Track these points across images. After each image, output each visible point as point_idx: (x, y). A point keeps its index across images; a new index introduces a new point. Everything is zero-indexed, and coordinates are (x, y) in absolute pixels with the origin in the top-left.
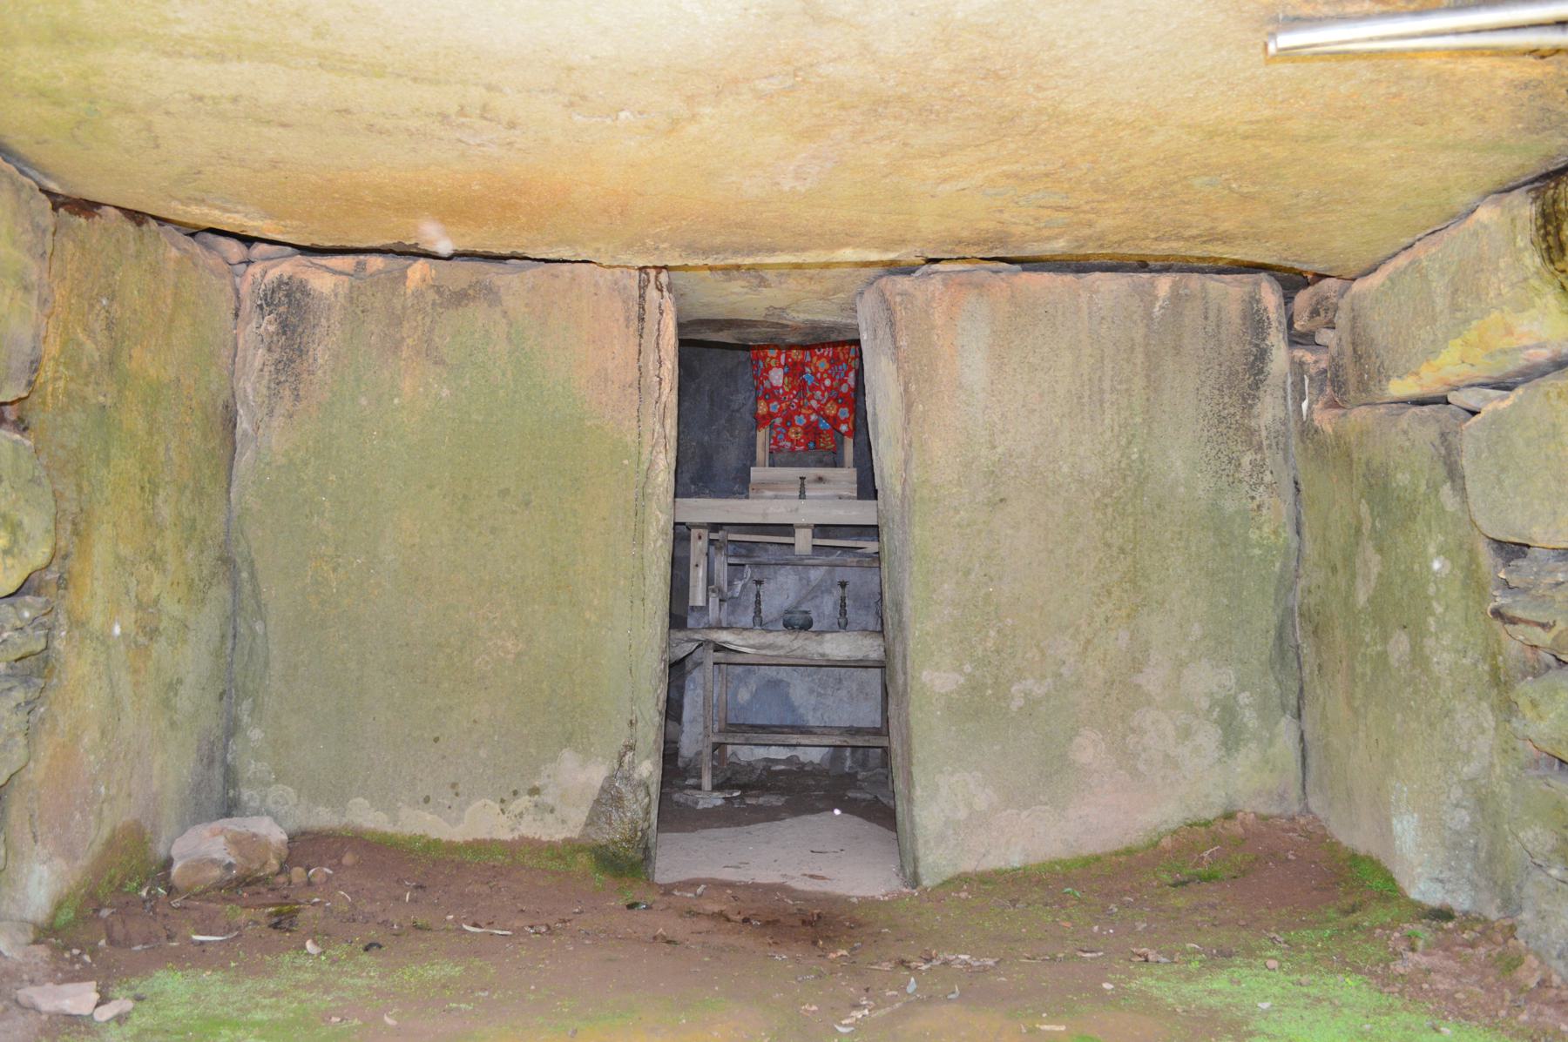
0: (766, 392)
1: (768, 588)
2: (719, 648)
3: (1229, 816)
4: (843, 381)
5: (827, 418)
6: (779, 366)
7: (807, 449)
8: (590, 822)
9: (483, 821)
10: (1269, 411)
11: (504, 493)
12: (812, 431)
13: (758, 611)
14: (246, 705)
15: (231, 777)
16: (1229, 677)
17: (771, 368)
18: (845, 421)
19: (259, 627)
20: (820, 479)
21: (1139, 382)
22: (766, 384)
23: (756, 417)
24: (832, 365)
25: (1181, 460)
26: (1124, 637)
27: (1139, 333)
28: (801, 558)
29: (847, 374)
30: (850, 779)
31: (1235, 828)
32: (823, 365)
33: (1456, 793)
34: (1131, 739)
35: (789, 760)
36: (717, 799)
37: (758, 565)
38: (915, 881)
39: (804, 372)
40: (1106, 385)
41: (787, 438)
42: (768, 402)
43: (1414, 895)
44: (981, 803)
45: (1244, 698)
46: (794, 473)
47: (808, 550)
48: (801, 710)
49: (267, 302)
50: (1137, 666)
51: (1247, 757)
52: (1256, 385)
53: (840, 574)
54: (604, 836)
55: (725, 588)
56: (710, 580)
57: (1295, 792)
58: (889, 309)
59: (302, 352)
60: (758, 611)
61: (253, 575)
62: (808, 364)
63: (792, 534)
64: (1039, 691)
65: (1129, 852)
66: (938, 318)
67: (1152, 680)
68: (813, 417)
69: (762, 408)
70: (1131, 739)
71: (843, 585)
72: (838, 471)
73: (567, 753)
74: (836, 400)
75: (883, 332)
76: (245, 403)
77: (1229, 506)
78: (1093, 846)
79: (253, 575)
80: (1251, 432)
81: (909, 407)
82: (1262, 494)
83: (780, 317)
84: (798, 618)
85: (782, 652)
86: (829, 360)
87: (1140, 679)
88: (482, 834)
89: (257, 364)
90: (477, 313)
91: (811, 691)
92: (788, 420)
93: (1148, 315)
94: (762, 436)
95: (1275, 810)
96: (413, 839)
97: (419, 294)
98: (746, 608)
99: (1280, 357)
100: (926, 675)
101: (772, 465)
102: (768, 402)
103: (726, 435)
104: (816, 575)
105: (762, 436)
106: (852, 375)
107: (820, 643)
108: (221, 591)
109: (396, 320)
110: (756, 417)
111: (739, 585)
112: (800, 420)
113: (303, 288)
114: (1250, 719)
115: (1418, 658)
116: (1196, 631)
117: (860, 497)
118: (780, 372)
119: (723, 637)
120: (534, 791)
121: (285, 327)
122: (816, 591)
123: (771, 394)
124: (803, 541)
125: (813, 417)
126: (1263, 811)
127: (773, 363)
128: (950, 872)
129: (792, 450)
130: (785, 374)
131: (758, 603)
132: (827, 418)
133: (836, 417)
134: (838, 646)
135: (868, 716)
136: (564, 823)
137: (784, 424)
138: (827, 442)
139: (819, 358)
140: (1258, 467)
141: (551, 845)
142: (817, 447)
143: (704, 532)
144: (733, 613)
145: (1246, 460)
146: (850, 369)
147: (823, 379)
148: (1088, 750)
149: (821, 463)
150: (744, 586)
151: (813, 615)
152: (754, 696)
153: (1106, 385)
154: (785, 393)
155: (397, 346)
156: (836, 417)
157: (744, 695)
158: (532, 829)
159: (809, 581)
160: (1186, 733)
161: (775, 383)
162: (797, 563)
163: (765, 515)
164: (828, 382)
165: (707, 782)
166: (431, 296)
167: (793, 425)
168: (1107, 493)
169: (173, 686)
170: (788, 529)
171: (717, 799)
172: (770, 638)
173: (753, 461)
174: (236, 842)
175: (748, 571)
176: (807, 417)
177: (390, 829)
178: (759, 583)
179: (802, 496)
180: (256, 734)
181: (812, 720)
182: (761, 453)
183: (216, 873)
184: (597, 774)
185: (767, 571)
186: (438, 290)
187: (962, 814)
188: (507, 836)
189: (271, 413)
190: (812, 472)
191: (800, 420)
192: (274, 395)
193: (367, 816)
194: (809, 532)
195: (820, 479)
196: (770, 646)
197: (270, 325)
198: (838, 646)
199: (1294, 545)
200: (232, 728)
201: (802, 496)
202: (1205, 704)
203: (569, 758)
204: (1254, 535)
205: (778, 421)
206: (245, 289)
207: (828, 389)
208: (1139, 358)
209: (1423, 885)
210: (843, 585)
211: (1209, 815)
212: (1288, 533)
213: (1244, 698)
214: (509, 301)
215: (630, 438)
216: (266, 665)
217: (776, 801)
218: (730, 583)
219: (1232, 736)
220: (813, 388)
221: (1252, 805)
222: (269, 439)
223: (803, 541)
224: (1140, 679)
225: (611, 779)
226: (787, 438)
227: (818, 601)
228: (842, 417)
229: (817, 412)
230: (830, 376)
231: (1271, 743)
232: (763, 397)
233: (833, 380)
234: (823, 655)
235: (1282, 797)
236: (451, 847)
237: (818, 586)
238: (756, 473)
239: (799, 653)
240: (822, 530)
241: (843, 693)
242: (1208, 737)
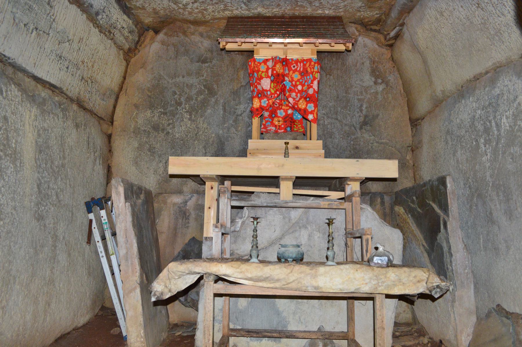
0: (259, 92)
1: (263, 223)
4: (309, 87)
5: (299, 110)
6: (268, 77)
7: (286, 131)
12: (289, 121)
17: (262, 78)
18: (312, 112)
20: (297, 148)
22: (259, 87)
24: (302, 76)
29: (312, 83)
32: (296, 76)
39: (284, 80)
41: (272, 124)
42: (260, 99)
46: (280, 143)
47: (290, 197)
48: (285, 314)
55: (229, 225)
62: (287, 75)
63: (278, 186)
68: (290, 112)
69: (256, 104)
74: (305, 98)
84: (292, 252)
85: (277, 285)
86: (300, 73)
92: (273, 113)
98: (244, 239)
102: (260, 99)
103: (233, 130)
105: (256, 121)
106: (316, 82)
107: (315, 276)
111: (239, 222)
112: (281, 113)
117: (326, 157)
118: (268, 81)
123: (262, 94)
125: (290, 112)
127: (263, 75)
129: (276, 132)
130: (272, 81)
131: (255, 237)
132: (299, 110)
133: (305, 110)
137: (270, 116)
138: (298, 127)
139: (294, 71)
142: (292, 130)
146: (315, 78)
147: (296, 86)
150: (243, 223)
154: (271, 94)
156: (305, 110)
159: (290, 220)
161: (265, 88)
163: (259, 169)
164: (300, 87)
167: (276, 116)
170: (273, 181)
173: (249, 136)
176: (286, 111)
181: (292, 327)
182: (255, 132)
190: (293, 143)
191: (281, 113)
194: (290, 184)
196: (265, 279)
205: (266, 114)
207: (300, 92)
218: (233, 221)
220: (290, 90)
226: (272, 124)
227: (297, 234)
228: (310, 110)
229: (293, 108)
230: (301, 83)
232: (257, 96)
233: (303, 86)
234: (316, 288)
237: (297, 222)
238: (252, 144)
239: (294, 285)
240: (300, 182)
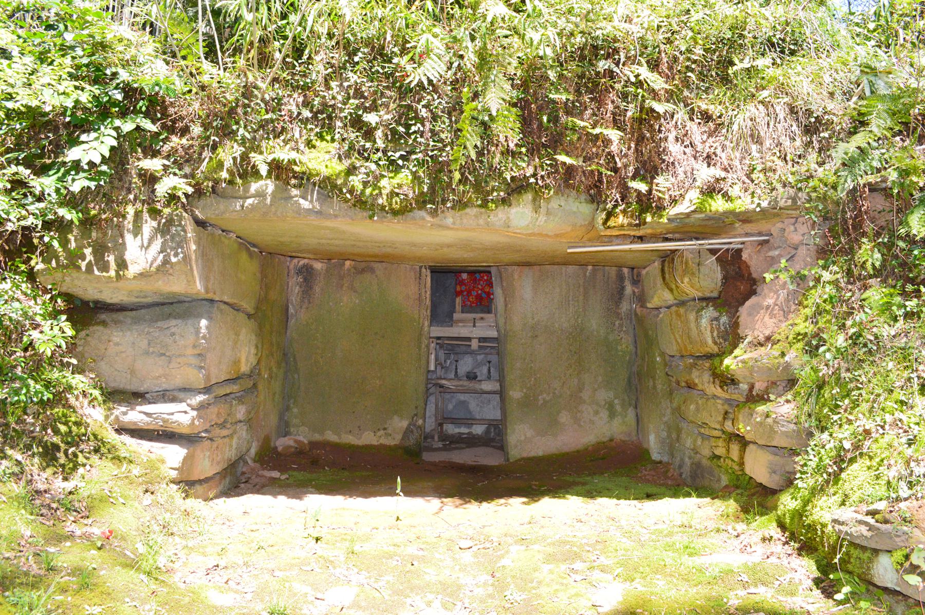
1: (461, 362)
2: (441, 386)
3: (611, 440)
8: (402, 439)
9: (368, 438)
10: (625, 307)
11: (376, 333)
13: (456, 372)
14: (292, 401)
15: (287, 424)
16: (611, 394)
19: (296, 376)
21: (581, 298)
23: (456, 292)
25: (595, 323)
26: (576, 380)
27: (581, 282)
28: (474, 351)
30: (493, 440)
31: (613, 444)
33: (662, 427)
34: (579, 415)
35: (468, 434)
36: (440, 445)
37: (457, 354)
38: (508, 460)
40: (570, 298)
43: (653, 458)
44: (529, 435)
45: (616, 401)
49: (300, 271)
50: (580, 390)
51: (617, 422)
52: (620, 299)
53: (489, 357)
54: (407, 444)
56: (436, 359)
57: (634, 433)
58: (500, 272)
59: (311, 288)
60: (456, 372)
61: (294, 359)
64: (548, 398)
65: (578, 451)
66: (516, 277)
67: (586, 395)
69: (458, 288)
70: (579, 415)
71: (489, 362)
72: (489, 315)
73: (395, 417)
75: (498, 279)
76: (292, 304)
77: (611, 338)
78: (566, 449)
79: (294, 359)
80: (618, 314)
81: (506, 306)
82: (622, 334)
83: (464, 500)
87: (582, 395)
88: (368, 443)
89: (296, 291)
90: (367, 277)
91: (478, 405)
92: (469, 292)
93: (585, 275)
94: (458, 300)
95: (627, 439)
96: (346, 444)
97: (349, 270)
99: (629, 289)
100: (511, 393)
101: (463, 312)
104: (480, 358)
108: (283, 365)
109: (341, 278)
110: (456, 292)
111: (449, 362)
112: (474, 293)
113: (312, 267)
114: (618, 408)
115: (655, 387)
116: (600, 379)
119: (444, 382)
120: (385, 429)
121: (305, 280)
122: (479, 365)
124: (475, 344)
126: (623, 439)
128: (519, 457)
134: (487, 386)
135: (496, 415)
136: (394, 440)
140: (621, 326)
141: (390, 446)
143: (435, 340)
144: (446, 373)
145: (617, 323)
148: (564, 417)
149: (483, 312)
151: (478, 374)
152: (454, 407)
153: (570, 298)
155: (342, 286)
157: (450, 407)
158: (383, 441)
160: (597, 413)
162: (472, 353)
165: (436, 438)
166: (353, 270)
168: (571, 334)
169: (274, 394)
170: (469, 339)
171: (440, 445)
172: (461, 383)
174: (296, 441)
175: (452, 356)
177: (338, 441)
178: (457, 361)
179: (474, 326)
180: (295, 410)
182: (458, 307)
183: (293, 450)
184: (405, 424)
185: (460, 356)
186: (355, 268)
187: (523, 438)
188: (375, 443)
189: (301, 307)
191: (474, 293)
192: (302, 301)
193: (331, 437)
195: (482, 318)
196: (461, 386)
197: (300, 279)
198: (487, 386)
199: (634, 351)
200: (288, 408)
201: (474, 326)
202: (603, 403)
203: (396, 419)
204: (619, 348)
206: (292, 267)
208: (581, 290)
209: (655, 456)
210: (489, 362)
211: (605, 440)
212: (631, 347)
213: (616, 401)
214: (378, 273)
215: (416, 316)
216: (299, 388)
217: (464, 446)
219: (612, 414)
221: (619, 437)
222: (300, 315)
223: (475, 344)
224: (582, 395)
225: (410, 425)
231: (626, 416)
235: (630, 435)
236: (358, 447)
238: (456, 316)
240: (481, 340)
241: (491, 406)
242: (604, 414)
